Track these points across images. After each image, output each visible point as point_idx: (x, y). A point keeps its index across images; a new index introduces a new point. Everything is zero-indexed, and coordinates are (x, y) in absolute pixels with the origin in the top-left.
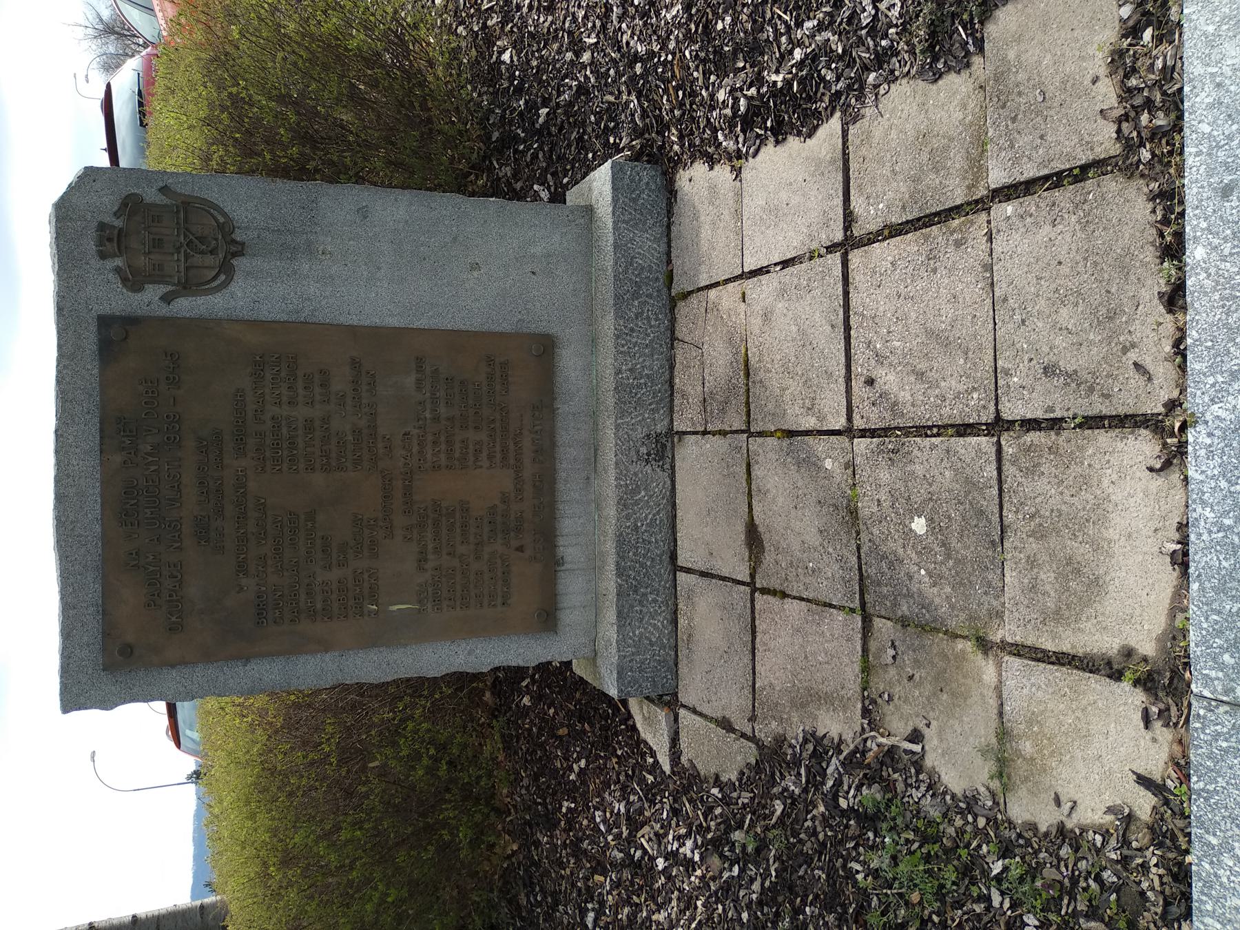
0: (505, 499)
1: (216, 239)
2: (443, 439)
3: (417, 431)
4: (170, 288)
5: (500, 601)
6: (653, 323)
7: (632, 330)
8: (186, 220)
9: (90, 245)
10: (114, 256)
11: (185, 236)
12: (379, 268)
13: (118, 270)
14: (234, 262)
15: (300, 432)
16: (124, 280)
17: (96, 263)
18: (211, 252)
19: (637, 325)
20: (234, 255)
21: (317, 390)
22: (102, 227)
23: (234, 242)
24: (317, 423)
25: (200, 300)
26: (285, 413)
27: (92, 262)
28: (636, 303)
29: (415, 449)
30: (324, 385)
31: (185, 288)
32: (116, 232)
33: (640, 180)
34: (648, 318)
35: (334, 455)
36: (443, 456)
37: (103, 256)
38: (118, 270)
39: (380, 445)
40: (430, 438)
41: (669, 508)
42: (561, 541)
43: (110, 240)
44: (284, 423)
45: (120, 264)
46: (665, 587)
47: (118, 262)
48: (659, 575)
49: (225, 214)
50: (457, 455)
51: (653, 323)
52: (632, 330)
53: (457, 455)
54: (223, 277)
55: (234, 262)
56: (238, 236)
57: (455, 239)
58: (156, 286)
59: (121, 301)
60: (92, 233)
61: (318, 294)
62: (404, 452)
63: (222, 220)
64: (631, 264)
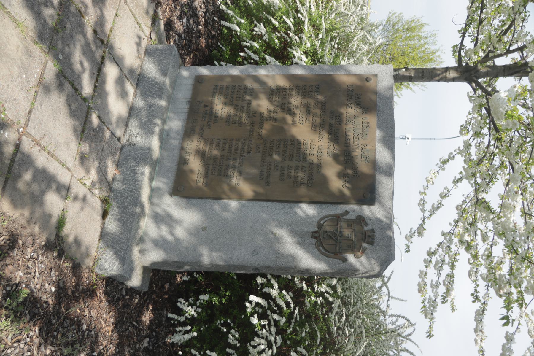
0: (209, 126)
1: (324, 238)
2: (233, 151)
3: (244, 155)
4: (345, 217)
5: (219, 87)
6: (120, 195)
7: (131, 191)
8: (336, 246)
9: (377, 235)
10: (368, 231)
11: (337, 239)
12: (251, 227)
13: (367, 225)
14: (316, 229)
15: (295, 155)
16: (364, 220)
17: (376, 228)
18: (326, 232)
19: (128, 194)
20: (316, 232)
21: (286, 172)
22: (371, 243)
23: (316, 238)
24: (287, 158)
25: (332, 212)
26: (301, 162)
27: (377, 228)
28: (126, 204)
29: (246, 147)
30: (282, 175)
31: (339, 217)
32: (366, 240)
33: (109, 264)
34: (121, 197)
35: (282, 146)
36: (234, 144)
37: (373, 231)
38: (367, 225)
39: (261, 149)
40: (239, 152)
41: (132, 114)
42: (186, 110)
43: (369, 236)
44: (301, 159)
45: (365, 227)
46: (142, 83)
47: (366, 228)
48: (104, 337)
49: (319, 250)
50: (227, 144)
51: (120, 195)
52: (131, 191)
53: (227, 144)
54: (322, 222)
55: (316, 229)
56: (314, 241)
57: (212, 242)
58: (351, 218)
59: (367, 211)
60: (377, 240)
61: (280, 216)
62: (251, 146)
63: (321, 248)
64: (124, 222)
